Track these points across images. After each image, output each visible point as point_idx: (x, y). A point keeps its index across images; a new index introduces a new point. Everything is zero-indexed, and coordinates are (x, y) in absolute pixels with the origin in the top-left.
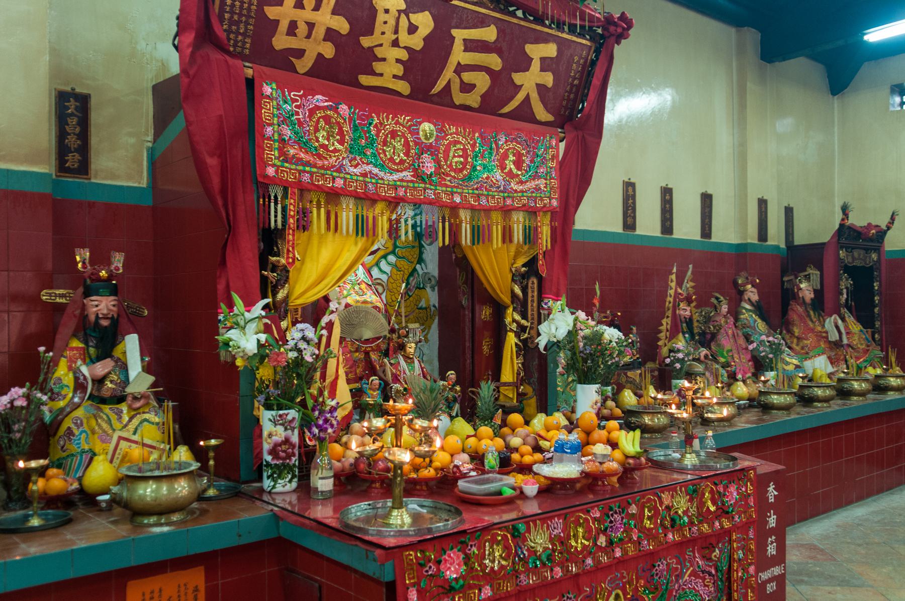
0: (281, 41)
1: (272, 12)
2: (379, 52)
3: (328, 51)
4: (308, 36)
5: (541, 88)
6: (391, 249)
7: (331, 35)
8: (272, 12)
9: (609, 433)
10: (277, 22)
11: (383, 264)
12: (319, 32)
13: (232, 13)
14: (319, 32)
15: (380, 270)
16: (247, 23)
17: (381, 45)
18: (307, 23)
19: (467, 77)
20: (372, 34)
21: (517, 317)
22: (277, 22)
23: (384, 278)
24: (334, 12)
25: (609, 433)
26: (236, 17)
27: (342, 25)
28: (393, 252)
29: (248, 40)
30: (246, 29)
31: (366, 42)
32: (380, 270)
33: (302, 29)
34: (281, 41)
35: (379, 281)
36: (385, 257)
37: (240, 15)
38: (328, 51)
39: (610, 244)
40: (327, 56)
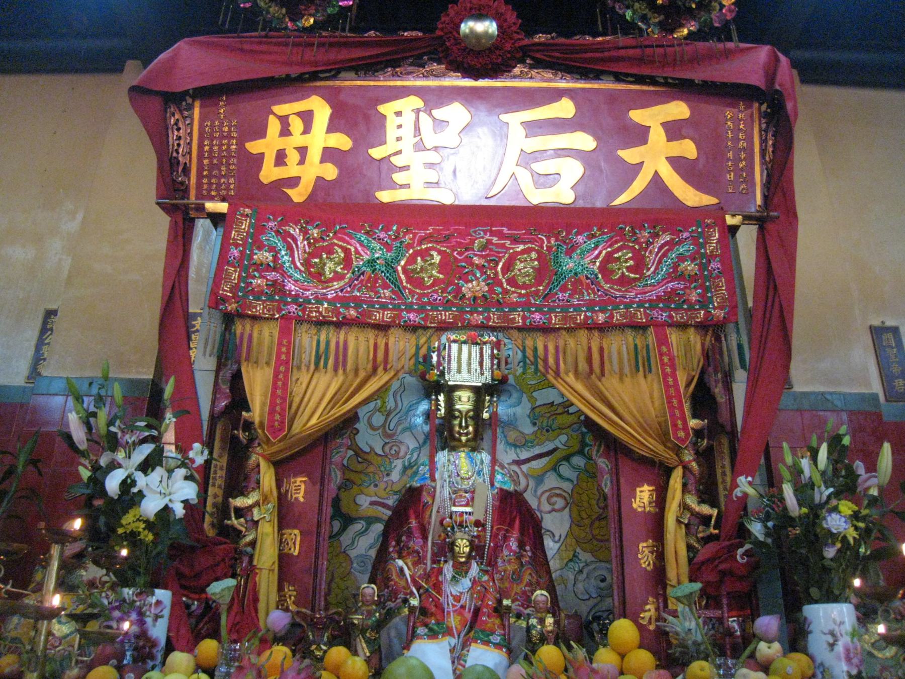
0: (269, 173)
1: (254, 147)
2: (397, 161)
3: (330, 172)
4: (302, 162)
5: (676, 163)
6: (577, 448)
7: (329, 154)
8: (254, 147)
9: (622, 656)
10: (262, 155)
11: (565, 470)
12: (315, 155)
13: (211, 158)
14: (315, 155)
15: (560, 476)
16: (228, 164)
17: (399, 152)
18: (297, 149)
19: (541, 167)
20: (385, 143)
21: (692, 501)
22: (262, 155)
23: (567, 486)
24: (331, 129)
25: (622, 656)
26: (215, 161)
27: (341, 141)
28: (580, 452)
29: (232, 180)
30: (228, 169)
31: (377, 153)
32: (560, 476)
33: (293, 157)
34: (269, 173)
35: (558, 492)
36: (567, 458)
37: (220, 158)
38: (330, 172)
39: (285, 103)
40: (329, 178)
